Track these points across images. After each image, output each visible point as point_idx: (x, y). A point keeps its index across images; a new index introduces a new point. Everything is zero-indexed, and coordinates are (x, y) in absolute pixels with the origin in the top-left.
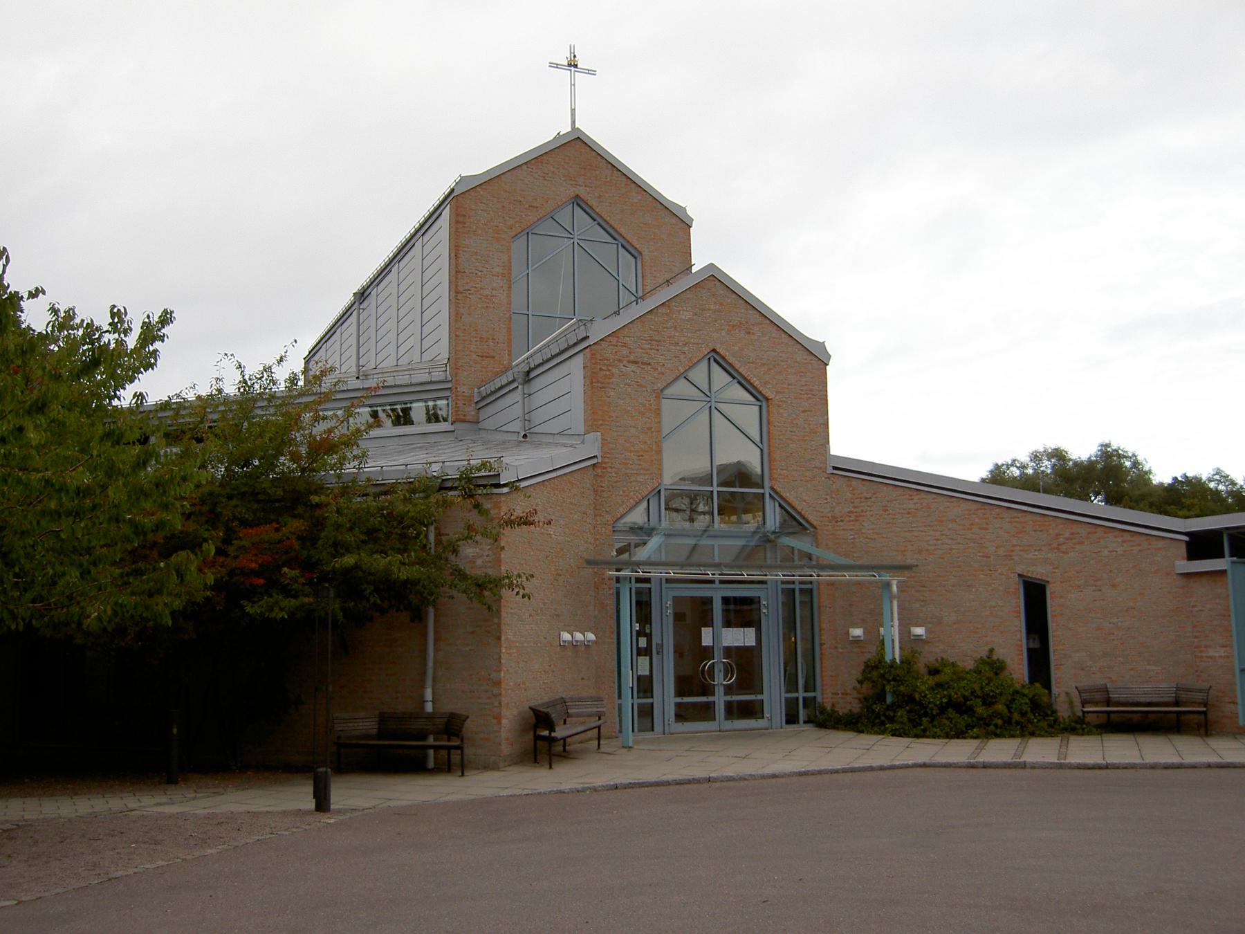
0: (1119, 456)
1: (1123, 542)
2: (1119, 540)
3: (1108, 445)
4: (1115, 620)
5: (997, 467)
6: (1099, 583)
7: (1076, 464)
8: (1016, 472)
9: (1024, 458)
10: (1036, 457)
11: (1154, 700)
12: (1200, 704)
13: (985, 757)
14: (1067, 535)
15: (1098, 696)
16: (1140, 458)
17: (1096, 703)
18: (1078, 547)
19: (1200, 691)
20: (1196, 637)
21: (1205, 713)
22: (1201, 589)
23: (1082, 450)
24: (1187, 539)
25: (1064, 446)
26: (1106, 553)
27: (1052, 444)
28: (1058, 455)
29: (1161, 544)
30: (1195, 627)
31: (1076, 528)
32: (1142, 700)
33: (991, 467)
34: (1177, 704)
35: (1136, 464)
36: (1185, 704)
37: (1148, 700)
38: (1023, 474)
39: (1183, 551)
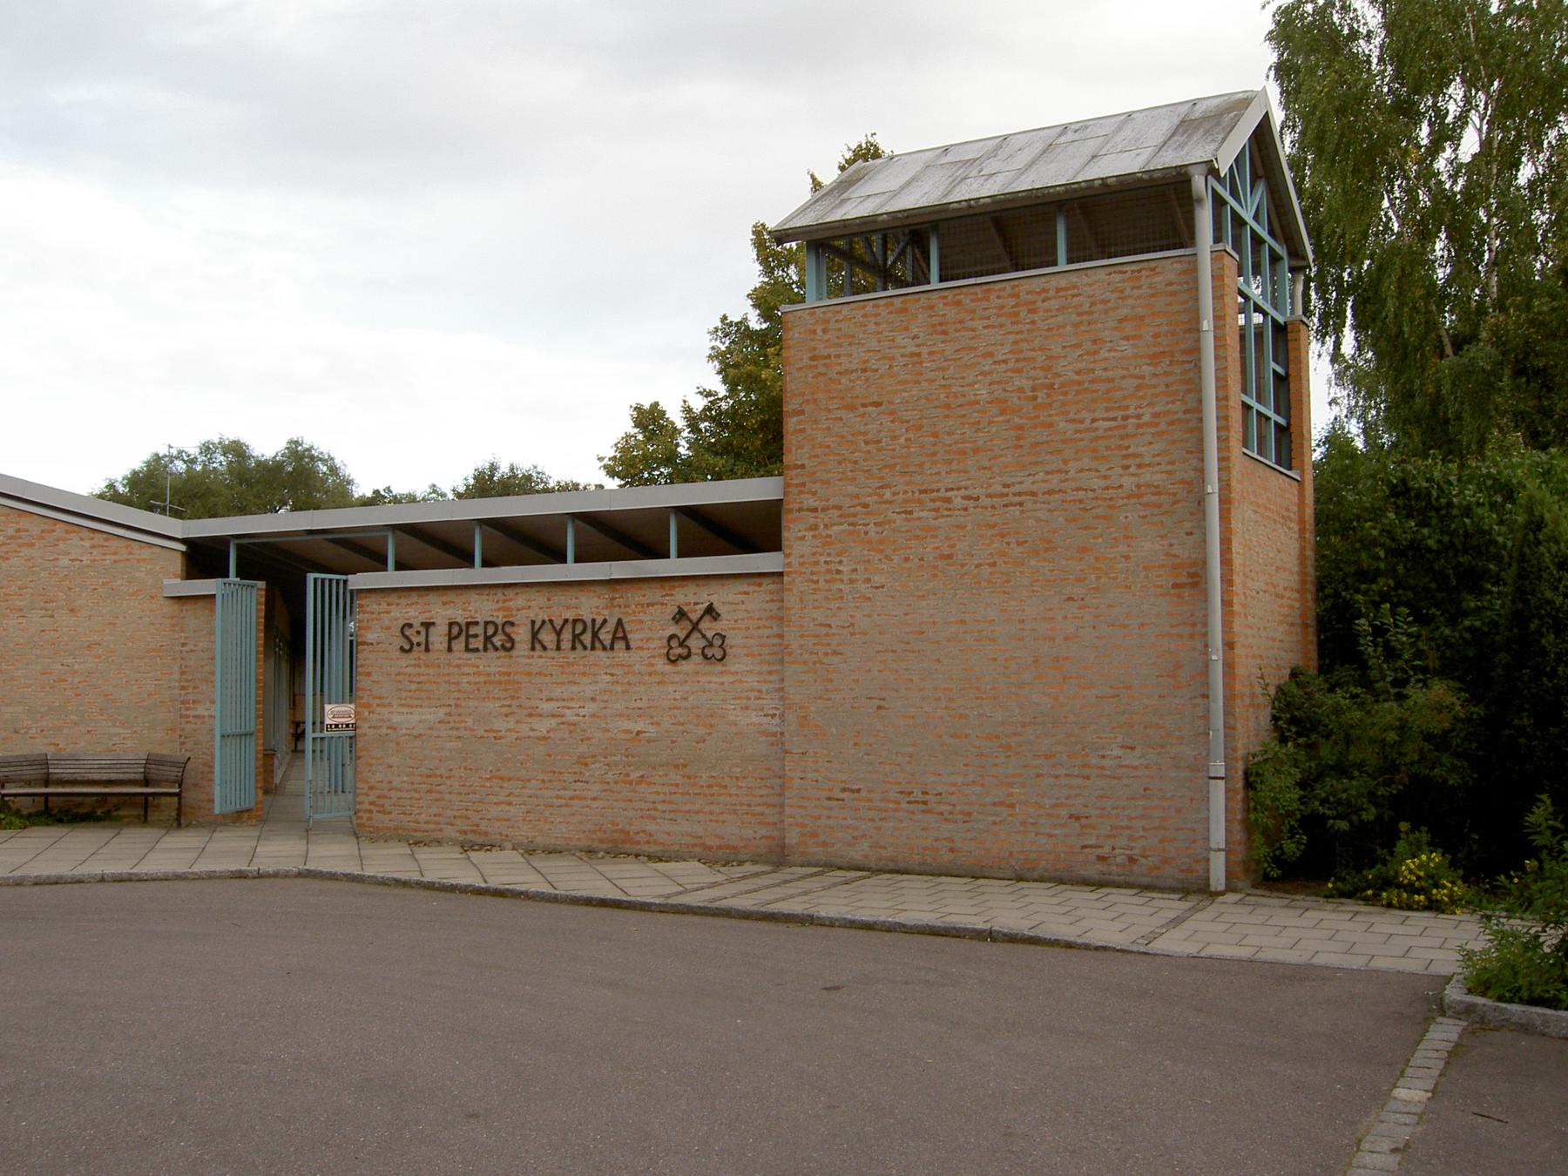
0: (312, 458)
1: (93, 547)
2: (87, 544)
3: (296, 443)
4: (70, 660)
5: (157, 458)
6: (53, 605)
7: (259, 463)
8: (180, 466)
9: (194, 451)
10: (207, 449)
11: (114, 777)
12: (172, 783)
13: (150, 866)
14: (11, 532)
15: (29, 772)
16: (338, 462)
17: (29, 783)
18: (25, 551)
19: (174, 764)
20: (183, 688)
21: (178, 795)
22: (193, 618)
23: (266, 446)
24: (183, 548)
25: (245, 438)
26: (65, 561)
27: (230, 435)
28: (237, 450)
29: (146, 553)
30: (183, 673)
31: (24, 522)
32: (96, 777)
33: (147, 456)
34: (47, 783)
35: (334, 470)
36: (158, 783)
37: (105, 777)
38: (189, 470)
39: (177, 564)
